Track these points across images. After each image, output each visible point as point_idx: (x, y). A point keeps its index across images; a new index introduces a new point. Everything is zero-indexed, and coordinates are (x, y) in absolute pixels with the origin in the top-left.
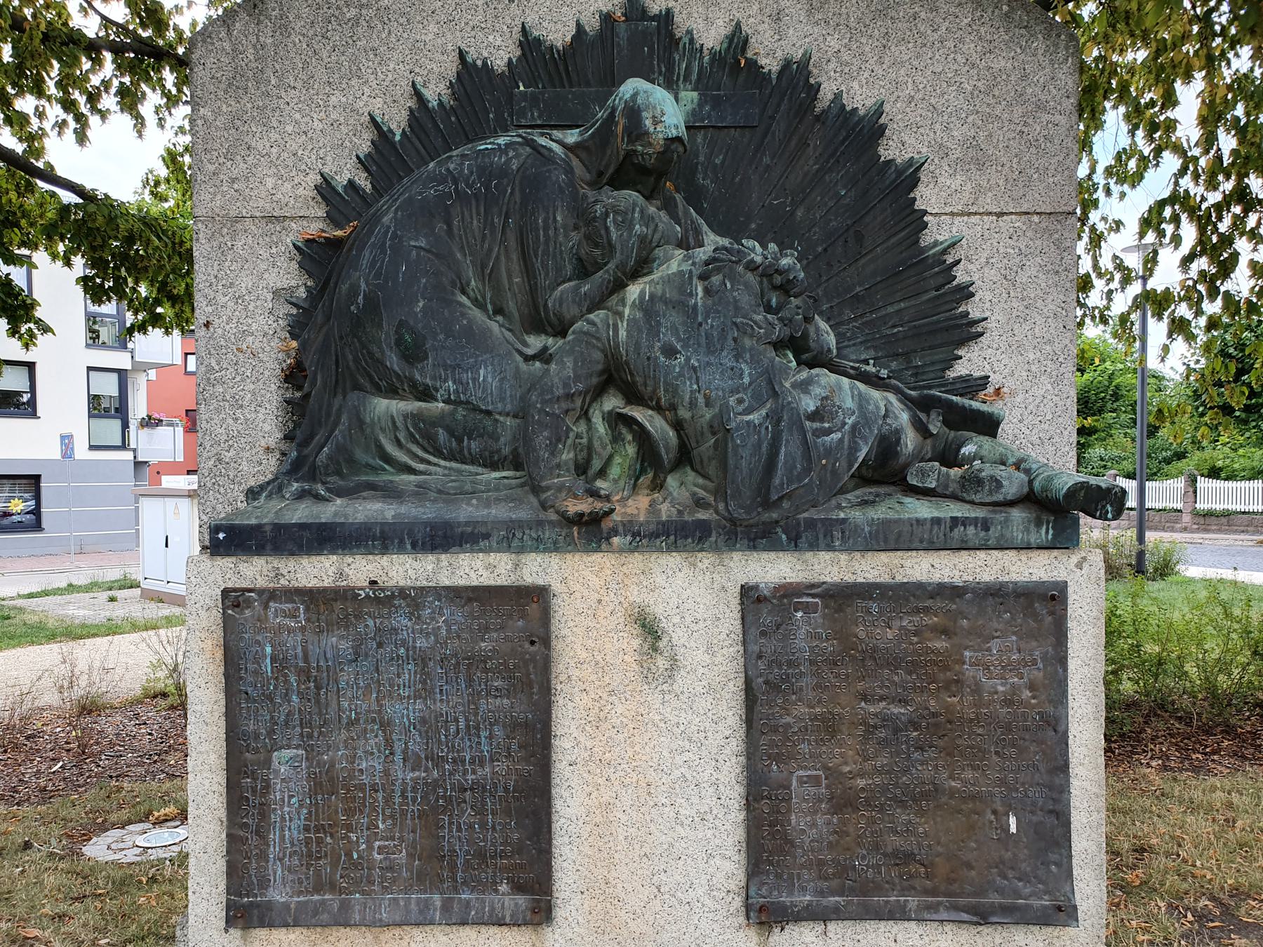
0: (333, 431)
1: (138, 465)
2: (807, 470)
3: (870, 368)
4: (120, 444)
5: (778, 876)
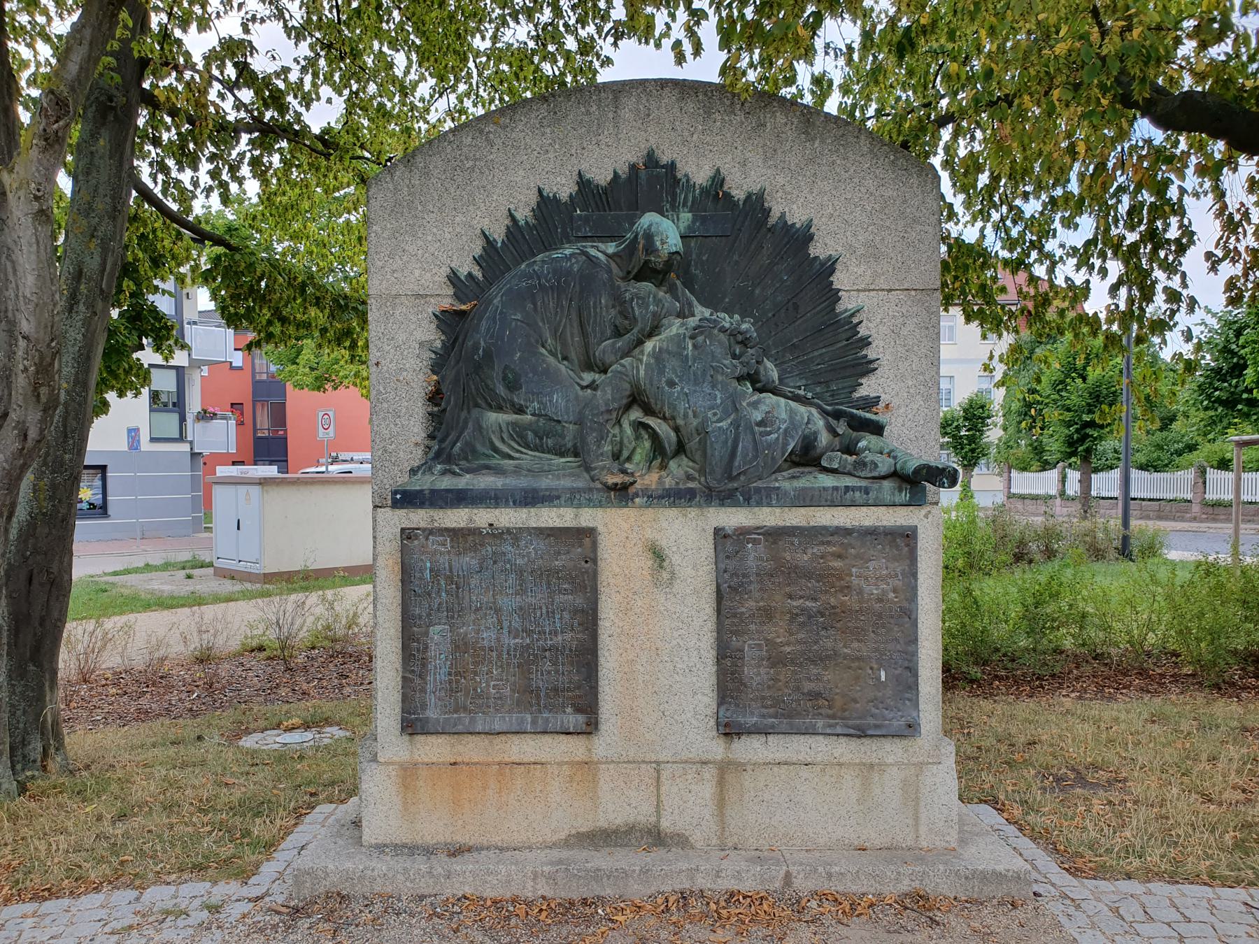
0: (461, 433)
1: (194, 455)
2: (756, 457)
3: (802, 392)
4: (177, 436)
5: (737, 705)
